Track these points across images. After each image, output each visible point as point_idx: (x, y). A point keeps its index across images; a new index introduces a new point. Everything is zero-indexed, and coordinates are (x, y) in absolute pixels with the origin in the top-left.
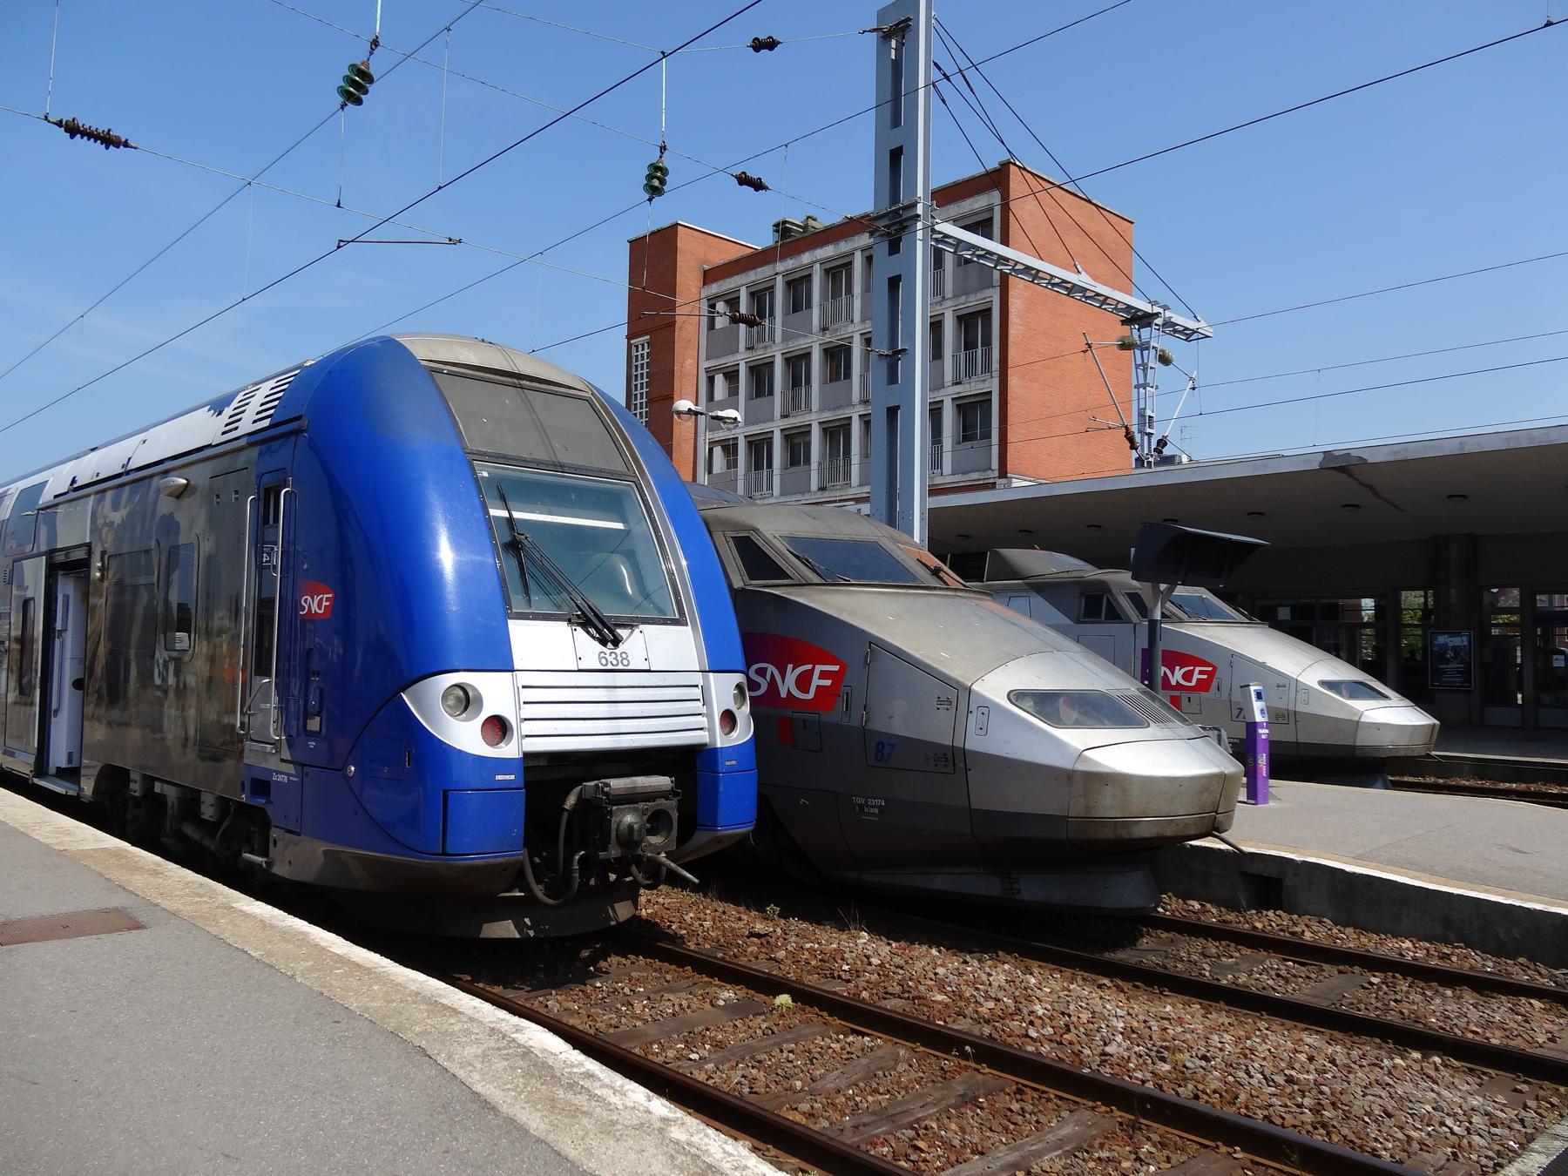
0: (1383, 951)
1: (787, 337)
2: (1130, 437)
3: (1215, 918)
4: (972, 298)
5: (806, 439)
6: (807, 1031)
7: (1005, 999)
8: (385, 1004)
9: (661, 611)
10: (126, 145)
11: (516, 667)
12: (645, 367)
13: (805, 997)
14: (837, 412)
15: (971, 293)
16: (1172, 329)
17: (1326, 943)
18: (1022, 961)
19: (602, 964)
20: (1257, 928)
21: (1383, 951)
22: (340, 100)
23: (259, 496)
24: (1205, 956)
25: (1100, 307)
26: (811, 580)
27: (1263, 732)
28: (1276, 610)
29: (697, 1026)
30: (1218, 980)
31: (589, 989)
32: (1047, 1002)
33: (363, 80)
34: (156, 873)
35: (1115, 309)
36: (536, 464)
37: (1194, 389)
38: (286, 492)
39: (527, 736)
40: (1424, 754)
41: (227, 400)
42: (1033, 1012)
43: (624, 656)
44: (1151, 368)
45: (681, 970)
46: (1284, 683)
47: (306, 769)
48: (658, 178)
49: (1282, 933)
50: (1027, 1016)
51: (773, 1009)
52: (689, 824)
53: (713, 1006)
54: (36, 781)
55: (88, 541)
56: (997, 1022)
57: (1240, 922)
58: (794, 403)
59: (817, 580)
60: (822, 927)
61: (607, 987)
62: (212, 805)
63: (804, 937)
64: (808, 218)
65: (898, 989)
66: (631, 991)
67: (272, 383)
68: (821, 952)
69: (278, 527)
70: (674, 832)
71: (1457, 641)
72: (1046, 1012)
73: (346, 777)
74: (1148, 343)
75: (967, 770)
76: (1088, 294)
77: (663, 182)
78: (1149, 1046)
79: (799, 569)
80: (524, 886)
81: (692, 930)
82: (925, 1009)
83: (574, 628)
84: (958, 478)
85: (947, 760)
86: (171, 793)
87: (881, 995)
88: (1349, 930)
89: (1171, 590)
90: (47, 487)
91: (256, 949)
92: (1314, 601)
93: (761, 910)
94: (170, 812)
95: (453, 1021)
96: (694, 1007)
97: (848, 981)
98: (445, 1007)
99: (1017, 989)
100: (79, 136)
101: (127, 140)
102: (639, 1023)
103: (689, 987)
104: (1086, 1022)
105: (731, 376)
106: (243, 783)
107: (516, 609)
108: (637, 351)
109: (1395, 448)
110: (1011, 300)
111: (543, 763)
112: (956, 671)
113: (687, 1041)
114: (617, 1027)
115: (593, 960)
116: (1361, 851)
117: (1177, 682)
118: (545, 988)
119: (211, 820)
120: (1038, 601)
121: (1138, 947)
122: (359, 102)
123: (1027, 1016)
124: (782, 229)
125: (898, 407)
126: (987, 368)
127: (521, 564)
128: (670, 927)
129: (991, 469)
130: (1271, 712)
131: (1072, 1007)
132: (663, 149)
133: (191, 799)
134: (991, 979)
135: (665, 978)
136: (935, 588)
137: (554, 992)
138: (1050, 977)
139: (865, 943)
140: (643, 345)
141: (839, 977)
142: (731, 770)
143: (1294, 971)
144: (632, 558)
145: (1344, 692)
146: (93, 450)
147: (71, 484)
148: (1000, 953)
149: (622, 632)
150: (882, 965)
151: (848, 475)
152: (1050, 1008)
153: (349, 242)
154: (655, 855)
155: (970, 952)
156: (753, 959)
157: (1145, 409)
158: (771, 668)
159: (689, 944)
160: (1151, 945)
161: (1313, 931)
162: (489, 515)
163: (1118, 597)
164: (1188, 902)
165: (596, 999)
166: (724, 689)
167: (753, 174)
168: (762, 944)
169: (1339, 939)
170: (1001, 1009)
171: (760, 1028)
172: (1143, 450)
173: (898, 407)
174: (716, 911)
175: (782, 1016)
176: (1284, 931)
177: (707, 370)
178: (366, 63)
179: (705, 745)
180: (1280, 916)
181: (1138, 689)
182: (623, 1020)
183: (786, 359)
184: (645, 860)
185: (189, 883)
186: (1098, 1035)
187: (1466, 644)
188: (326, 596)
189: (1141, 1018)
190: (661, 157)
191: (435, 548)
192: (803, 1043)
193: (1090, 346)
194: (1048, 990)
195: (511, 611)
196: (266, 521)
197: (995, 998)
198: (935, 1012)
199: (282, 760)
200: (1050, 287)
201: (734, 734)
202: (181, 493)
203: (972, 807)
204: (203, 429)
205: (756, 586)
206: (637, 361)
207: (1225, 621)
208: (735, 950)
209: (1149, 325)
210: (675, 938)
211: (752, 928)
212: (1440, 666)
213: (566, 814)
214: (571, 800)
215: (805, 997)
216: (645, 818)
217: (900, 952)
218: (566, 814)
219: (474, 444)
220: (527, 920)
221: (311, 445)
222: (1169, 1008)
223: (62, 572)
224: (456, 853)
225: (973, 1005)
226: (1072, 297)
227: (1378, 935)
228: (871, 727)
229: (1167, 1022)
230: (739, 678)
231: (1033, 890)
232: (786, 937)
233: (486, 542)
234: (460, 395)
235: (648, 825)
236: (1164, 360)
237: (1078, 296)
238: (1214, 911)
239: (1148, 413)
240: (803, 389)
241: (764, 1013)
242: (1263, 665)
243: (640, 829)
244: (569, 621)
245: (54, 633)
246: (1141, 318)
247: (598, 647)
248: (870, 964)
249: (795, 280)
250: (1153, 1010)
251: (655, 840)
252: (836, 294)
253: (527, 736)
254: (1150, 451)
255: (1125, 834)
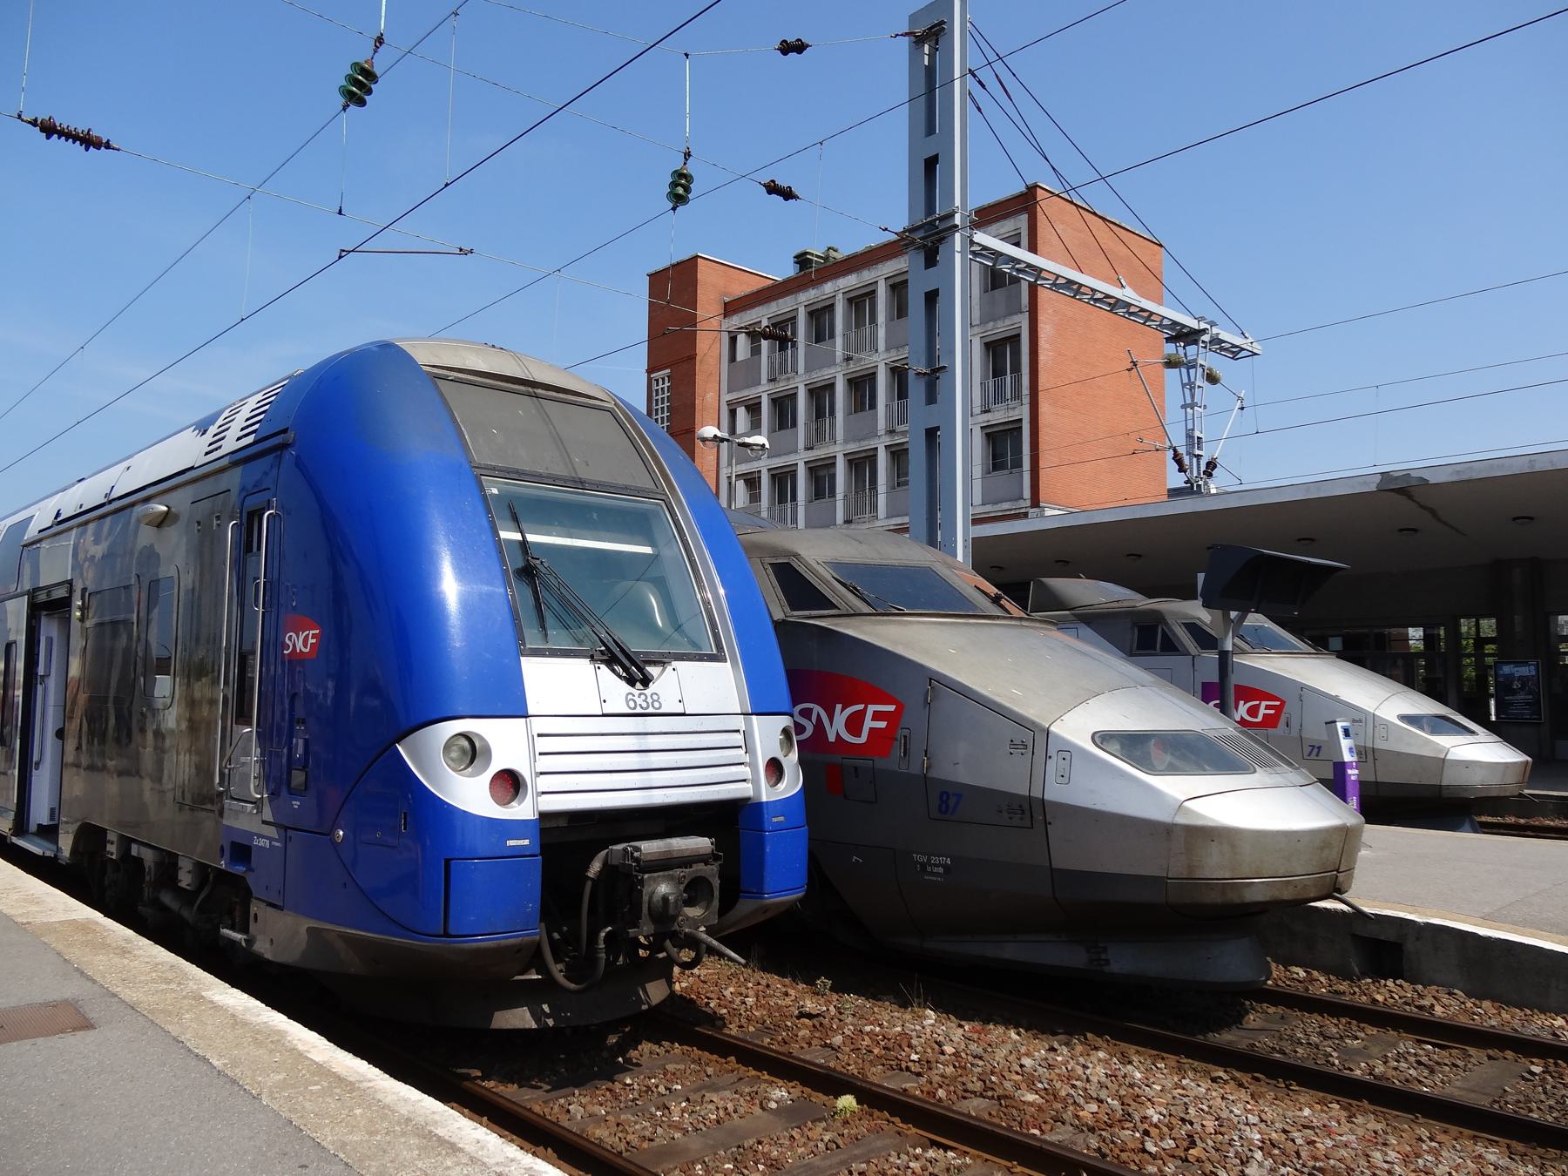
0: (1533, 1030)
1: (809, 369)
2: (1178, 459)
3: (1324, 987)
4: (1000, 324)
5: (831, 471)
6: (879, 1144)
7: (1109, 1100)
8: (367, 1137)
9: (694, 645)
10: (108, 146)
11: (530, 713)
12: (666, 401)
13: (872, 1098)
14: (863, 443)
15: (999, 319)
16: (1218, 346)
17: (1464, 1020)
18: (1115, 1045)
19: (633, 1054)
20: (1378, 1001)
21: (1533, 1030)
22: (342, 101)
23: (241, 521)
24: (1326, 1037)
25: (1144, 324)
26: (859, 609)
27: (1352, 773)
28: (1327, 640)
29: (747, 1138)
30: (1352, 1070)
31: (617, 1087)
32: (1160, 1104)
33: (366, 79)
34: (124, 952)
35: (1159, 325)
36: (553, 480)
37: (1242, 408)
38: (270, 514)
39: (543, 793)
40: (1517, 794)
41: (211, 420)
42: (1146, 1118)
43: (655, 697)
44: (1199, 387)
45: (724, 1060)
46: (1360, 718)
47: (290, 833)
48: (682, 185)
49: (1407, 1008)
50: (1139, 1124)
51: (835, 1113)
52: (732, 892)
53: (763, 1108)
54: (15, 840)
55: (69, 578)
56: (1103, 1130)
57: (1355, 993)
58: (818, 435)
59: (867, 609)
60: (880, 1003)
61: (638, 1084)
62: (189, 872)
63: (862, 1017)
64: (829, 248)
65: (978, 1086)
66: (666, 1089)
67: (260, 397)
68: (884, 1037)
69: (260, 555)
70: (716, 903)
71: (1524, 671)
72: (1162, 1117)
73: (334, 844)
74: (1195, 360)
75: (1046, 823)
76: (1132, 310)
77: (687, 189)
78: (1298, 1166)
79: (846, 597)
80: (542, 968)
81: (734, 1009)
82: (1015, 1112)
83: (597, 665)
84: (988, 508)
85: (1023, 812)
86: (148, 856)
87: (960, 1093)
88: (1487, 1004)
89: (1242, 618)
90: (33, 522)
91: (220, 1056)
92: (1366, 631)
93: (810, 982)
94: (147, 878)
95: (449, 1163)
96: (741, 1110)
97: (919, 1074)
98: (441, 1141)
99: (1120, 1085)
100: (56, 136)
101: (108, 140)
102: (677, 1135)
103: (734, 1083)
104: (1213, 1132)
105: (754, 408)
106: (222, 847)
107: (530, 644)
108: (657, 385)
109: (1458, 468)
110: (1041, 325)
111: (563, 823)
112: (1031, 710)
113: (736, 1159)
114: (652, 1140)
115: (622, 1048)
116: (1487, 910)
117: (1242, 717)
118: (567, 1087)
119: (188, 888)
120: (1086, 631)
121: (1245, 1026)
122: (362, 103)
123: (1139, 1124)
124: (802, 260)
125: (938, 428)
126: (1017, 395)
127: (535, 593)
128: (708, 1004)
129: (1022, 498)
130: (1362, 752)
131: (1192, 1111)
132: (687, 155)
133: (168, 863)
134: (1088, 1072)
135: (705, 1072)
136: (998, 617)
137: (577, 1092)
138: (1153, 1067)
139: (933, 1025)
140: (663, 379)
141: (908, 1069)
142: (779, 828)
143: (1436, 1057)
144: (1072, 297)
145: (1426, 727)
146: (80, 481)
147: (56, 518)
148: (1089, 1035)
149: (653, 670)
150: (956, 1054)
151: (874, 507)
152: (1165, 1112)
153: (350, 252)
154: (694, 931)
155: (1054, 1034)
156: (805, 1046)
157: (1193, 430)
158: (817, 709)
159: (730, 1026)
160: (1259, 1024)
161: (1445, 1006)
162: (499, 538)
163: (1173, 627)
164: (1289, 968)
165: (626, 1101)
166: (768, 733)
167: (782, 182)
168: (814, 1026)
169: (1477, 1015)
170: (1107, 1114)
171: (822, 1140)
172: (1192, 472)
173: (938, 428)
174: (759, 984)
175: (846, 1122)
176: (1409, 1004)
177: (729, 403)
178: (370, 61)
179: (749, 799)
180: (1401, 986)
181: (1235, 729)
182: (659, 1130)
183: (809, 390)
184: (682, 936)
185: (158, 964)
186: (1231, 1149)
187: (1533, 673)
188: (312, 632)
189: (1279, 1125)
190: (685, 164)
191: (435, 576)
192: (875, 1161)
193: (1135, 364)
194: (1159, 1088)
195: (524, 646)
196: (249, 549)
197: (1097, 1099)
198: (1028, 1117)
199: (264, 822)
200: (1092, 302)
201: (782, 786)
202: (163, 521)
203: (1053, 866)
204: (187, 451)
205: (799, 617)
206: (657, 395)
207: (1293, 652)
208: (784, 1034)
209: (1195, 342)
210: (715, 1020)
211: (802, 1007)
212: (1506, 698)
213: (589, 884)
214: (595, 867)
215: (872, 1098)
216: (682, 887)
217: (975, 1036)
218: (589, 884)
219: (482, 456)
220: (546, 1007)
221: (298, 463)
222: (1307, 1112)
223: (45, 613)
224: (460, 933)
225: (1071, 1108)
226: (1116, 313)
227: (1522, 1010)
228: (933, 774)
229: (1311, 1132)
230: (784, 721)
231: (1123, 961)
232: (841, 1017)
233: (496, 568)
234: (464, 402)
235: (685, 895)
236: (1212, 379)
237: (1121, 311)
238: (1322, 979)
239: (1197, 434)
240: (827, 420)
241: (823, 1119)
242: (1336, 699)
243: (676, 901)
244: (592, 657)
245: (37, 679)
246: (1187, 335)
247: (624, 687)
248: (943, 1053)
249: (817, 310)
250: (1290, 1114)
251: (694, 912)
252: (859, 323)
253: (543, 793)
254: (1199, 474)
255: (1233, 897)
